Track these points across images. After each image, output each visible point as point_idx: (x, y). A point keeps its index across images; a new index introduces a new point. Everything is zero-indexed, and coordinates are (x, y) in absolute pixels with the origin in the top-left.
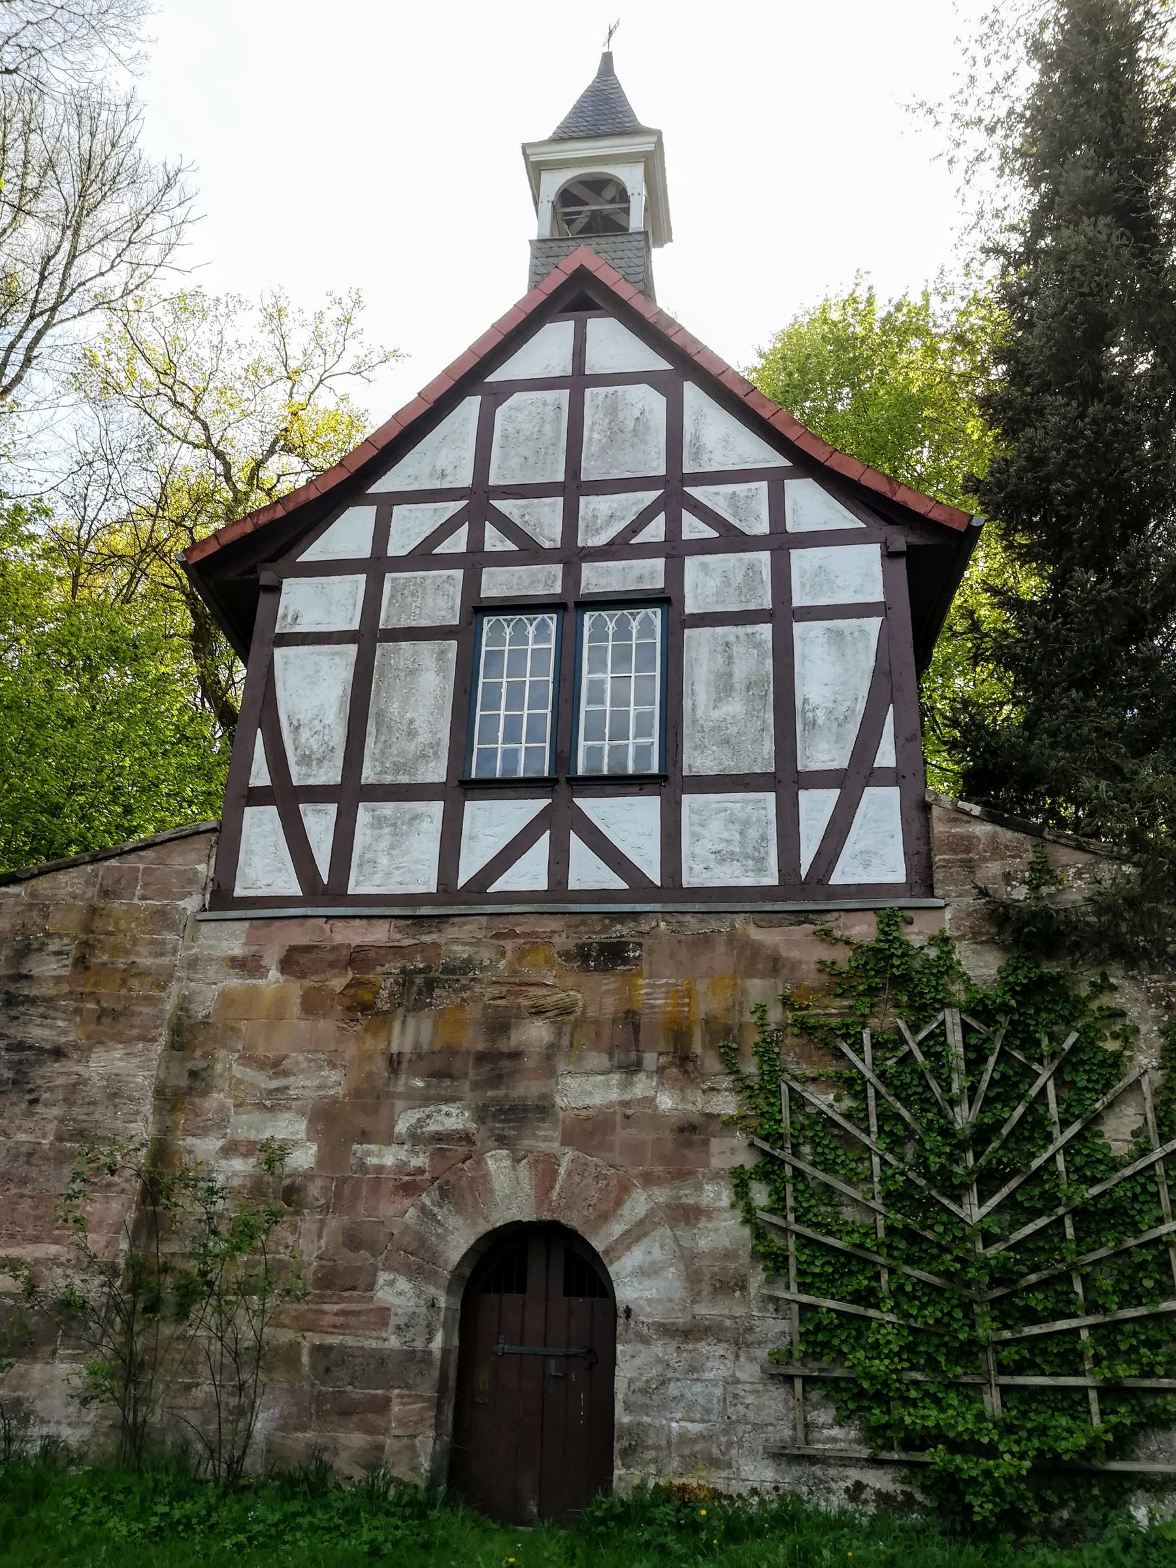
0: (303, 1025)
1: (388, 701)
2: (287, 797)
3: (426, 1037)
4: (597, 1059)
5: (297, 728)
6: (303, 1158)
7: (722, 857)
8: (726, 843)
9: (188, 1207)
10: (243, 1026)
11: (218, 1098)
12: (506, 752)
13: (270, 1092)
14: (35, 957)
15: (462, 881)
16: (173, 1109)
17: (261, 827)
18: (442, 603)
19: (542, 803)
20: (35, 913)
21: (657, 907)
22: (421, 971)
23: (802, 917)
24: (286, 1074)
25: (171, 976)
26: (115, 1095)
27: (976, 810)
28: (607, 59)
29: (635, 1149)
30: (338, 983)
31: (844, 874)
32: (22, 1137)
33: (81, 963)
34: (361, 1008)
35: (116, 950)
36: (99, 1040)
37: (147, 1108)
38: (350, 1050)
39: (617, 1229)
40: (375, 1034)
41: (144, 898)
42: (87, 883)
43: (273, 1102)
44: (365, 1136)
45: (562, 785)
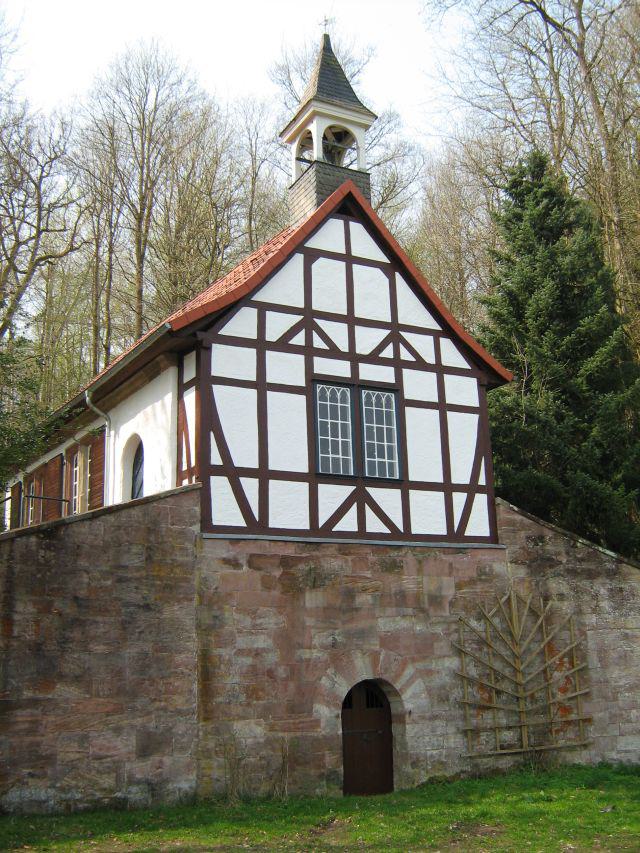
2: (234, 474)
6: (272, 658)
12: (389, 463)
17: (220, 486)
19: (352, 488)
27: (516, 508)
28: (327, 38)
44: (301, 646)
45: (361, 482)
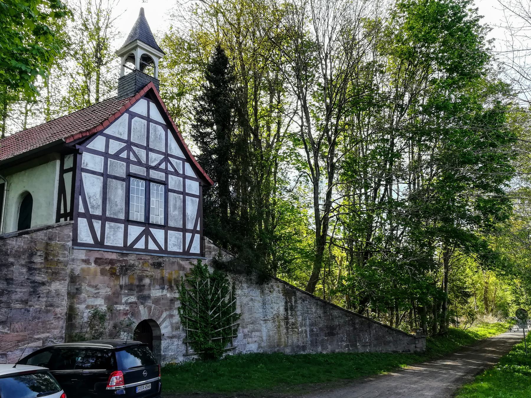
0: (101, 277)
1: (111, 195)
2: (90, 218)
3: (127, 281)
4: (157, 287)
5: (90, 198)
7: (174, 245)
8: (175, 241)
9: (78, 321)
10: (87, 277)
11: (83, 295)
13: (95, 293)
14: (35, 256)
15: (128, 245)
16: (73, 298)
18: (122, 171)
20: (33, 244)
21: (166, 255)
22: (124, 266)
23: (187, 259)
24: (98, 289)
25: (68, 263)
26: (58, 295)
27: (212, 242)
29: (164, 304)
30: (108, 268)
31: (191, 251)
32: (37, 307)
33: (46, 259)
34: (113, 274)
35: (54, 255)
36: (53, 280)
37: (66, 298)
38: (112, 284)
39: (161, 320)
40: (117, 280)
41: (59, 241)
42: (45, 236)
43: (96, 296)
44: (116, 303)
